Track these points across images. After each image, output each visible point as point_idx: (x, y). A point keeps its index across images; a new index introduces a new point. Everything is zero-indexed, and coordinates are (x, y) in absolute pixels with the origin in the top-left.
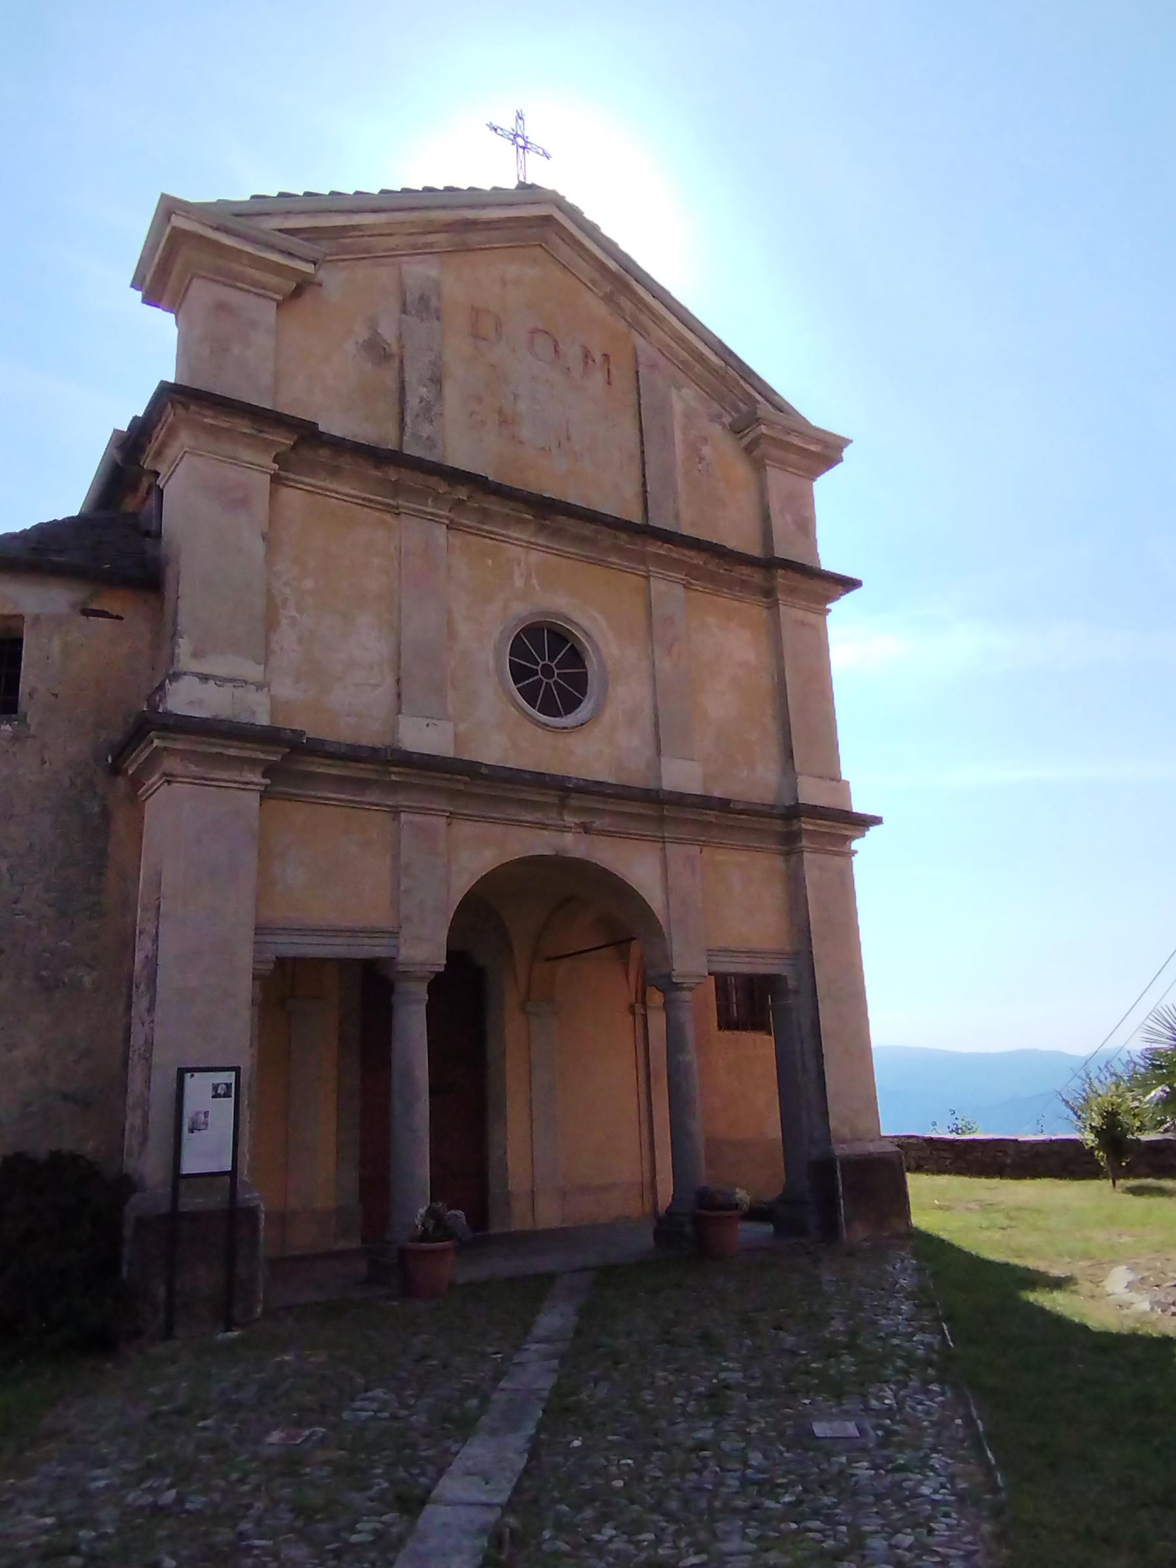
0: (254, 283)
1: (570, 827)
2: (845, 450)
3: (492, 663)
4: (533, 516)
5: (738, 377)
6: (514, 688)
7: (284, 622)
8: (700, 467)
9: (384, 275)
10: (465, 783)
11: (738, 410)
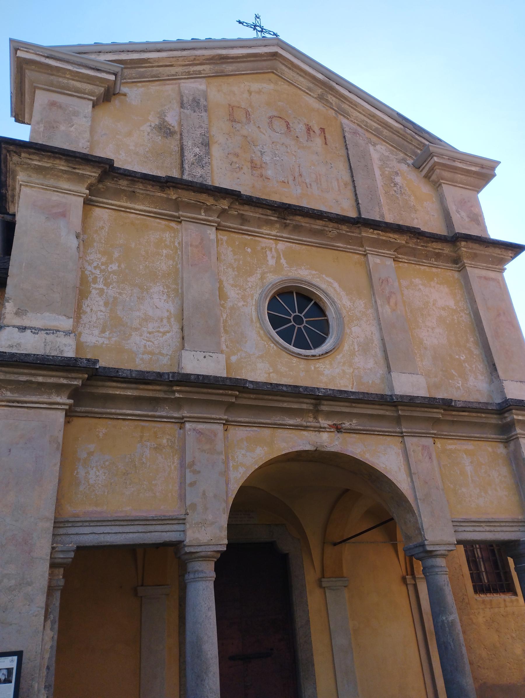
0: (78, 91)
1: (324, 428)
2: (496, 169)
3: (254, 314)
4: (278, 217)
5: (414, 134)
6: (273, 333)
7: (94, 292)
8: (395, 189)
9: (169, 89)
10: (236, 397)
11: (415, 154)
